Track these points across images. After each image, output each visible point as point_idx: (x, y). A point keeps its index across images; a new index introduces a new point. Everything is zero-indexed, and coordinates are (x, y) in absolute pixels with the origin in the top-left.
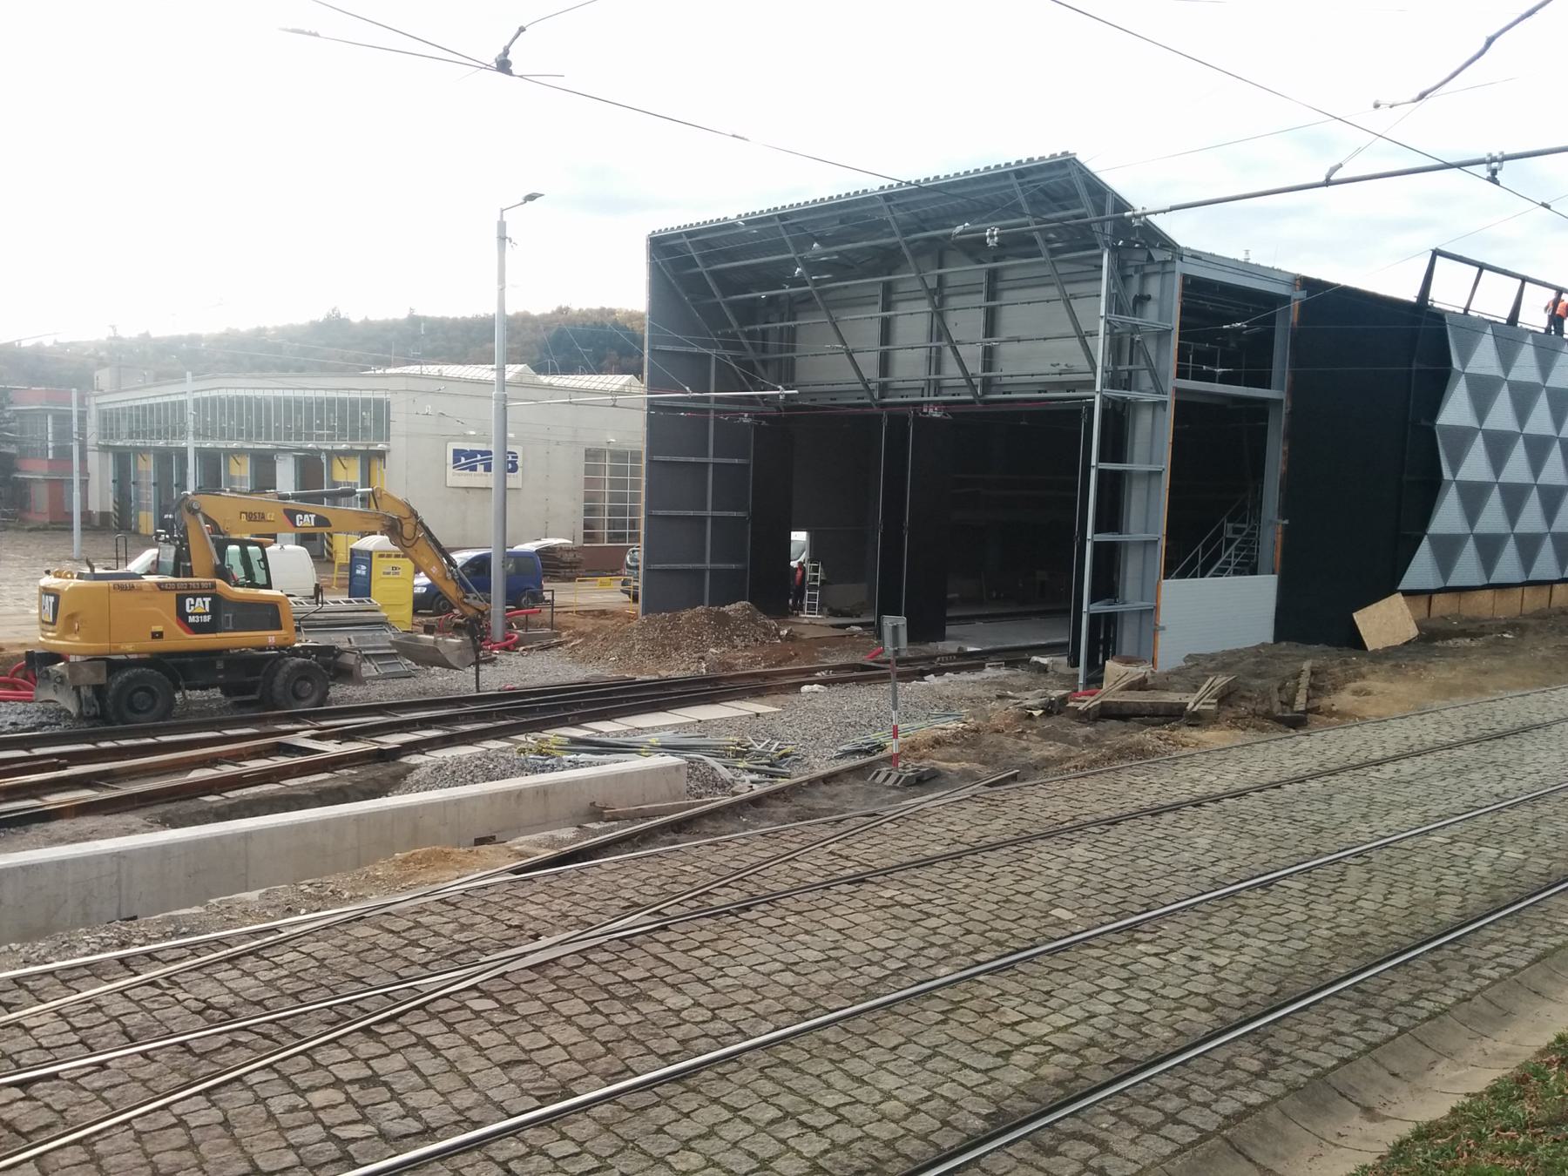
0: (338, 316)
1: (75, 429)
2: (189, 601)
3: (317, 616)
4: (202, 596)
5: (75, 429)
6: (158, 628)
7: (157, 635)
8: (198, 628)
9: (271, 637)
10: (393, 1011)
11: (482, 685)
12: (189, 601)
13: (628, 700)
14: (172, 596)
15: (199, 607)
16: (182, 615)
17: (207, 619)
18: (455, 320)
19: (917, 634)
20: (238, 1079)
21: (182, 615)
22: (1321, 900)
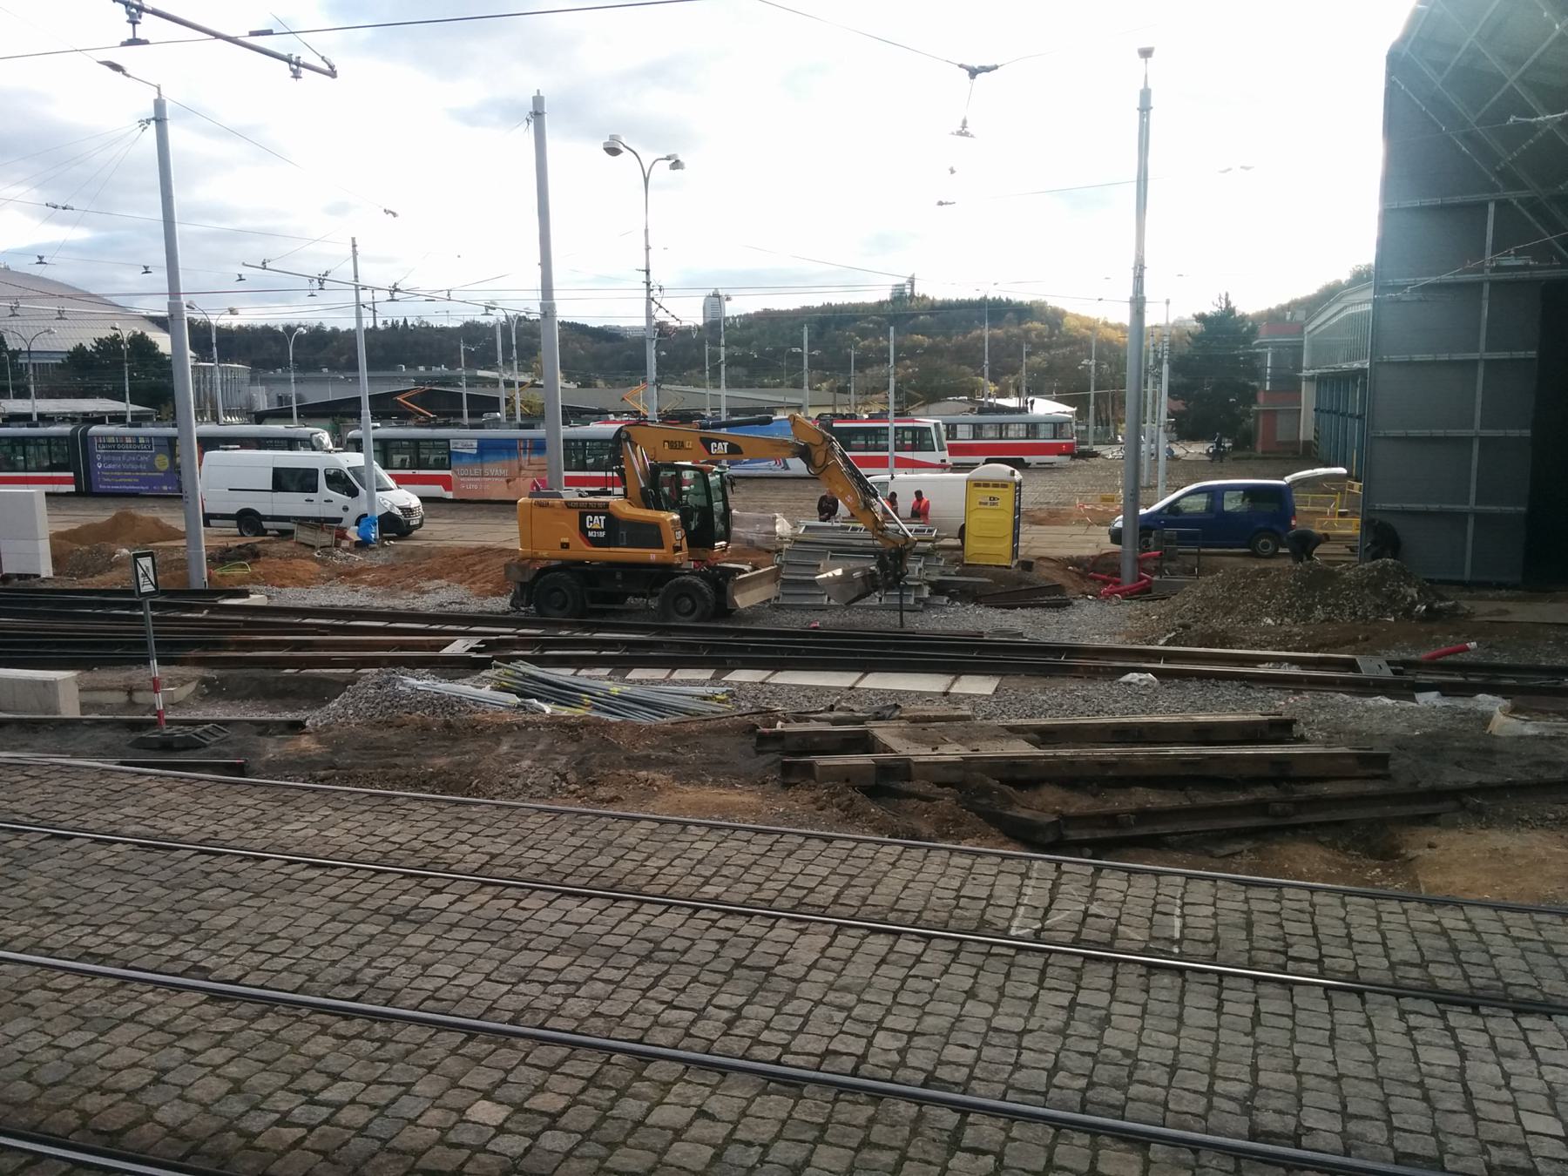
0: (1230, 311)
1: (480, 373)
2: (589, 518)
3: (855, 542)
4: (599, 514)
5: (480, 373)
6: (566, 540)
7: (565, 546)
8: (595, 542)
9: (653, 555)
10: (660, 1050)
11: (906, 624)
12: (589, 518)
13: (862, 654)
14: (576, 513)
15: (596, 522)
16: (584, 530)
17: (602, 534)
18: (757, 313)
19: (539, 611)
20: (1253, 1136)
21: (584, 530)
22: (1440, 1071)
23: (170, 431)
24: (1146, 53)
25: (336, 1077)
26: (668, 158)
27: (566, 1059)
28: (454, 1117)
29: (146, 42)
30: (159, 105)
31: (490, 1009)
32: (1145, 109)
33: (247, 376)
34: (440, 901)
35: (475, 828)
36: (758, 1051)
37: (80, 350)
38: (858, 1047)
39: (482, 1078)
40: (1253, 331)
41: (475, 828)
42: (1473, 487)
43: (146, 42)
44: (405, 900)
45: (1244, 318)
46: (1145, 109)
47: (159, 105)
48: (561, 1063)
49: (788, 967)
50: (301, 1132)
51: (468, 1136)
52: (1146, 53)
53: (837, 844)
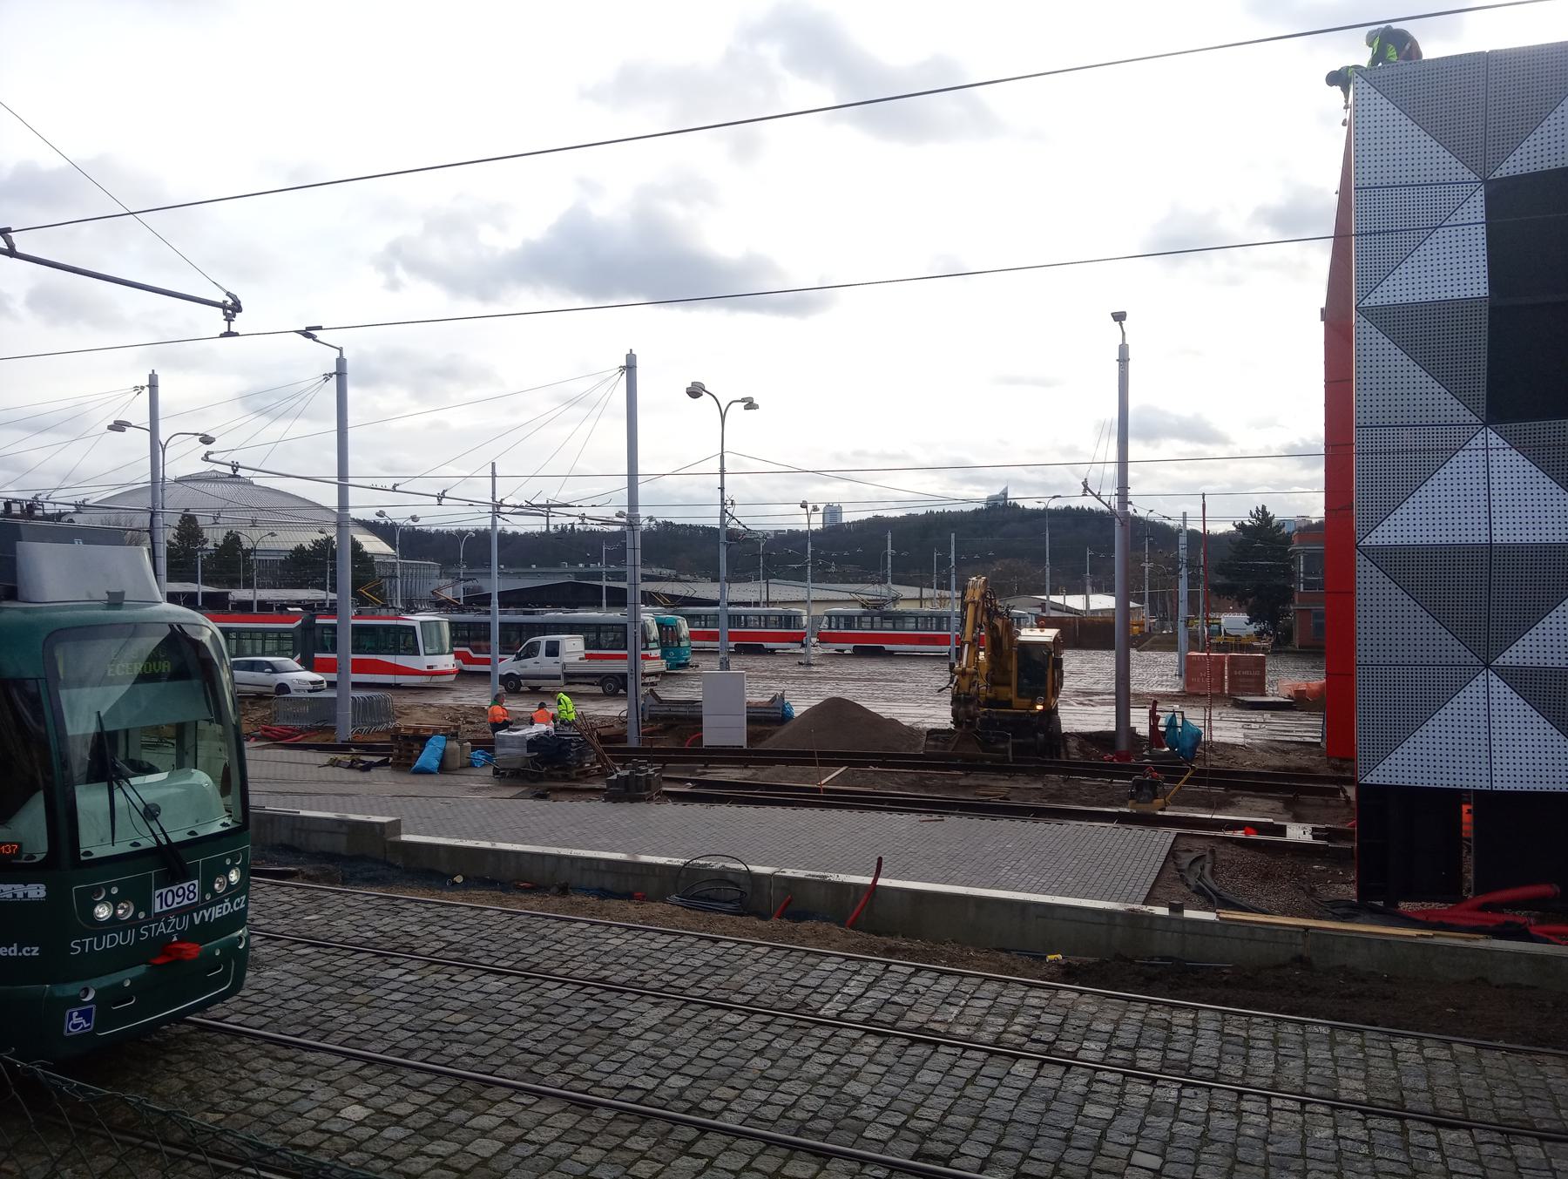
0: (1263, 515)
23: (334, 621)
24: (1119, 317)
25: (260, 1084)
26: (743, 400)
27: (431, 1082)
28: (331, 1114)
29: (236, 334)
30: (341, 362)
31: (393, 1047)
32: (1123, 360)
33: (437, 572)
34: (394, 973)
35: (445, 923)
36: (577, 1084)
37: (300, 550)
38: (651, 1083)
39: (360, 1091)
40: (1288, 539)
41: (445, 923)
42: (486, 845)
43: (236, 334)
44: (369, 972)
45: (1280, 526)
46: (1123, 360)
47: (341, 362)
48: (424, 1084)
49: (630, 1029)
50: (222, 1116)
51: (336, 1126)
52: (750, 405)
53: (722, 944)
